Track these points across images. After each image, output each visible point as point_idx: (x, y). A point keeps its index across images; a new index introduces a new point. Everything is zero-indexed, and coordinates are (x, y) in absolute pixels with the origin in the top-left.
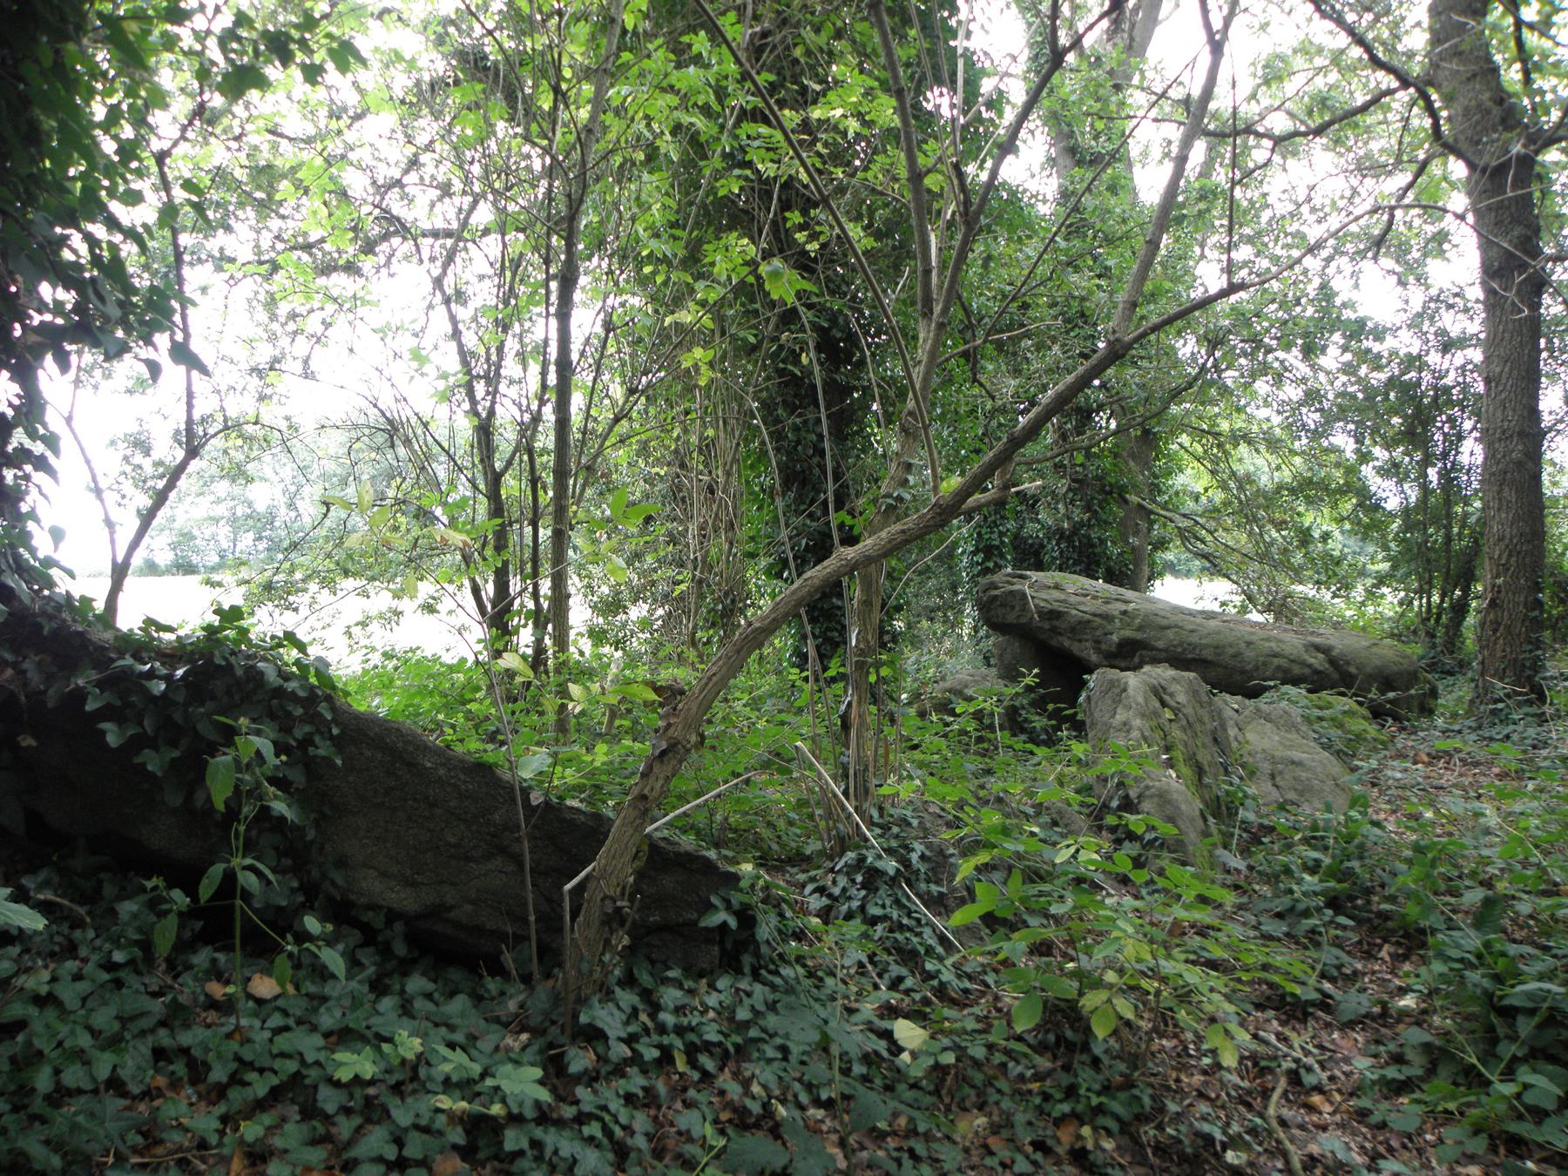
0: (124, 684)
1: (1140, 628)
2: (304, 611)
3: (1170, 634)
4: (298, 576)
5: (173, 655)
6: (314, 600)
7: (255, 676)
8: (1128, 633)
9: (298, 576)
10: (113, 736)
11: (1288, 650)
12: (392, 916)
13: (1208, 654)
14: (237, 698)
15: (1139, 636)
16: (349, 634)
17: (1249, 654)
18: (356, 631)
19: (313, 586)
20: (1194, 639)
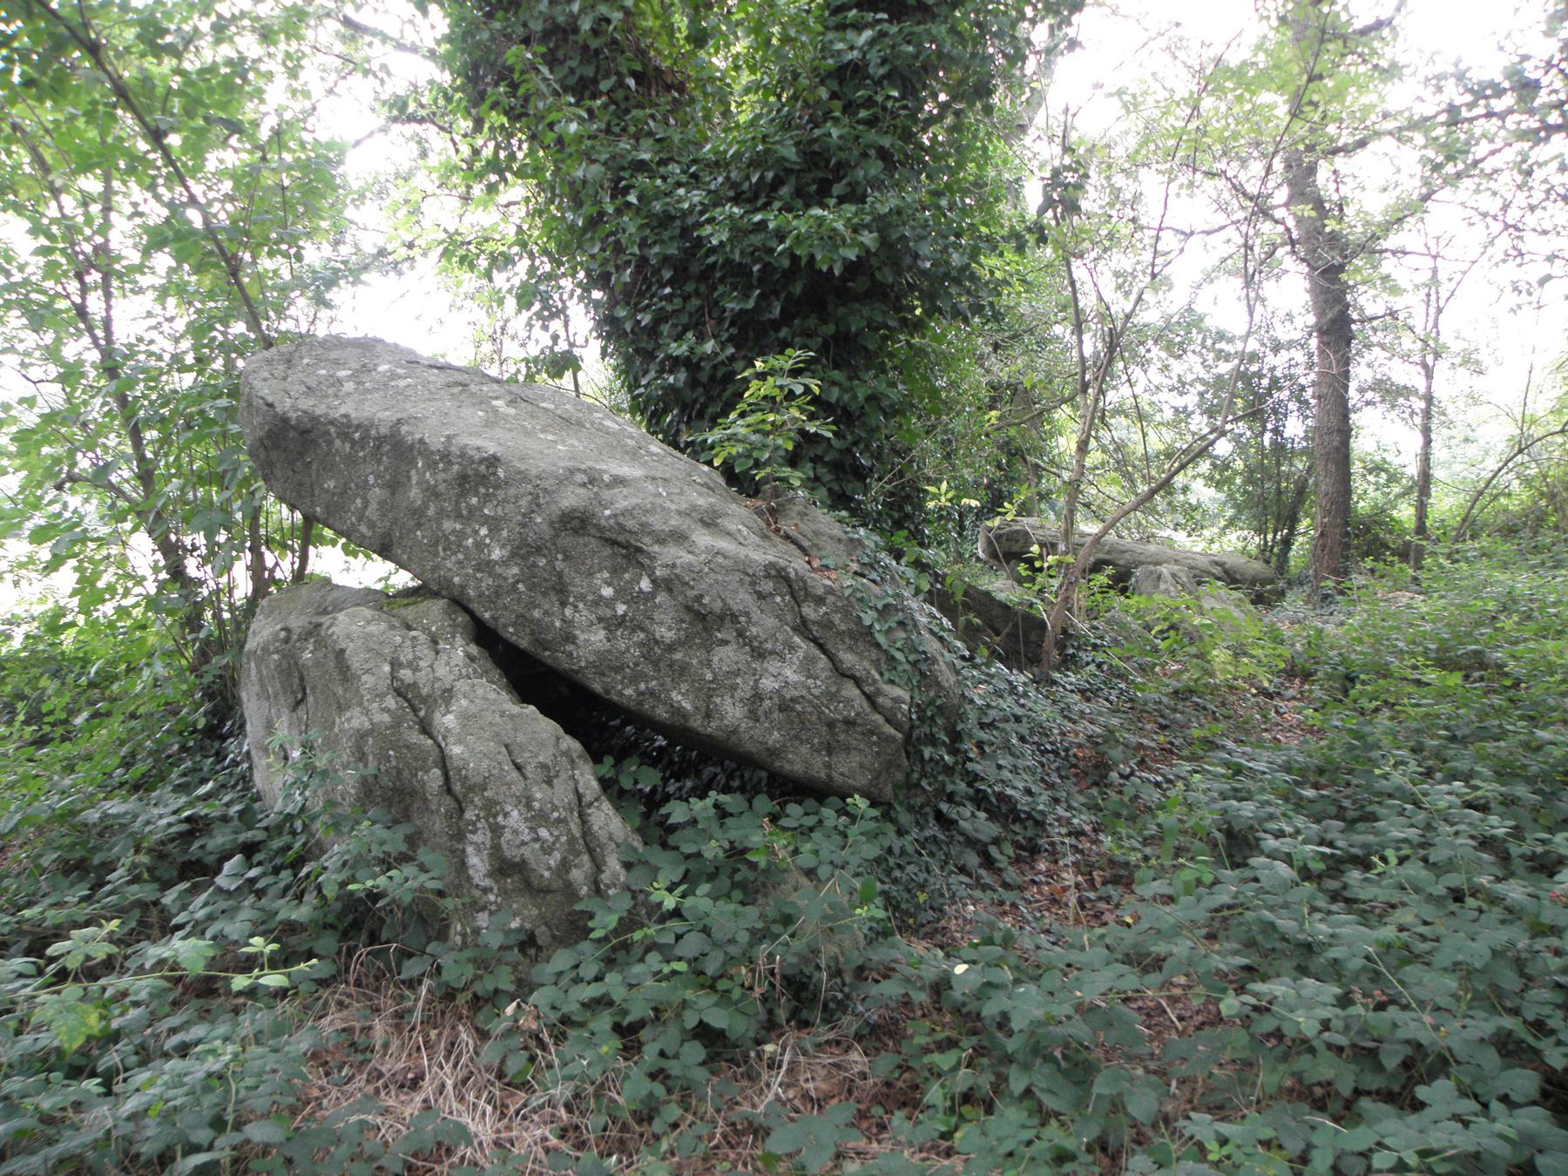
1: (1108, 552)
3: (1127, 555)
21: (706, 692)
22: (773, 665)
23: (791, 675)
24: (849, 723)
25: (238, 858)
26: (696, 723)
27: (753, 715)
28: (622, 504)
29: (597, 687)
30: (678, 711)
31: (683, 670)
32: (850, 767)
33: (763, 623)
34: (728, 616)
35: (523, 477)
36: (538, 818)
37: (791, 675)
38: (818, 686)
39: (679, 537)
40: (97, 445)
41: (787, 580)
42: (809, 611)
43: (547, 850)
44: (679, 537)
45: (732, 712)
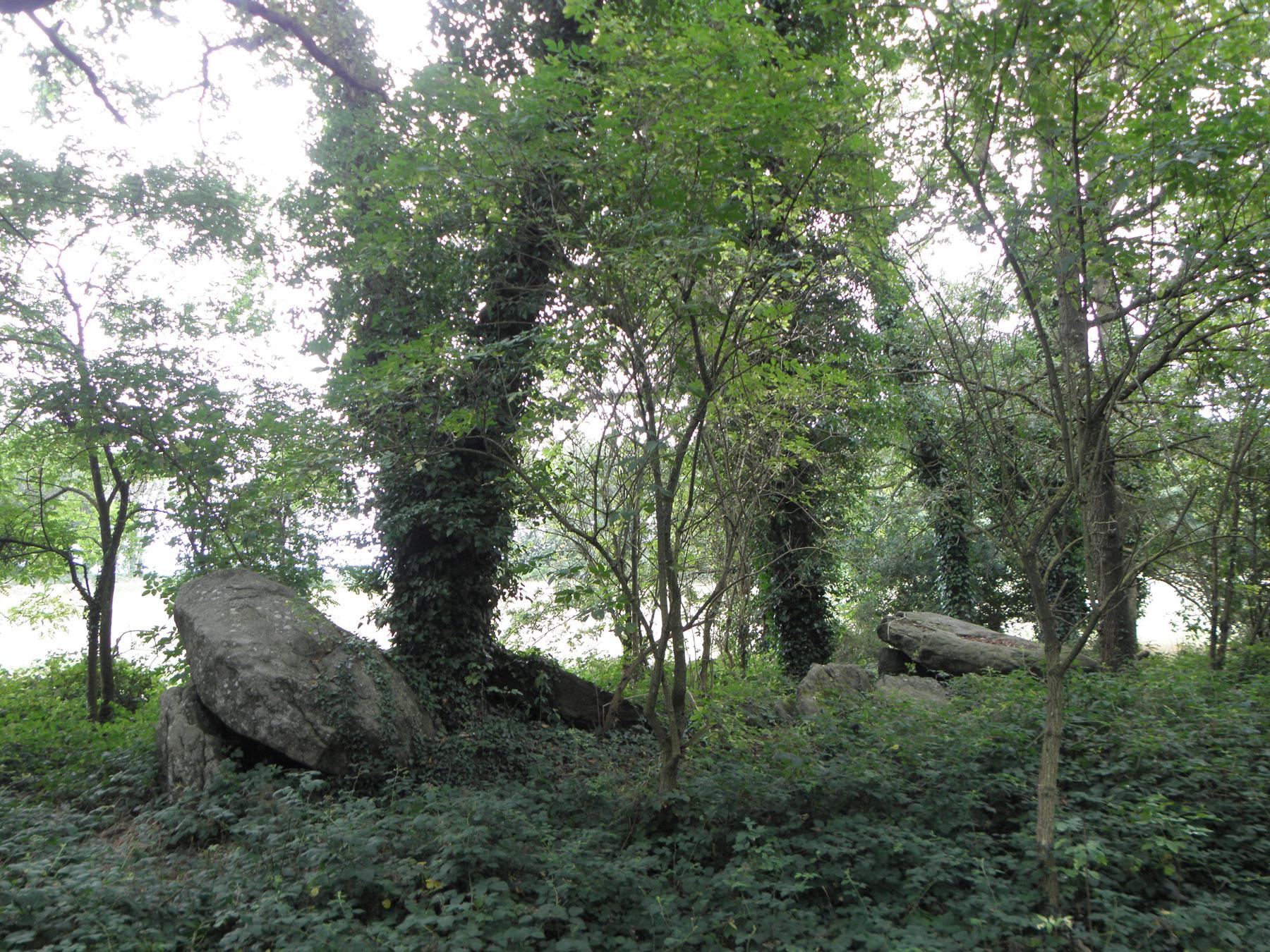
0: (516, 665)
1: (931, 645)
2: (545, 630)
3: (945, 647)
4: (541, 609)
5: (526, 658)
6: (550, 623)
7: (542, 663)
8: (925, 647)
9: (541, 609)
10: (514, 675)
11: (1002, 655)
12: (571, 718)
13: (962, 657)
14: (114, 871)
15: (930, 648)
16: (570, 642)
17: (982, 658)
18: (574, 640)
19: (549, 616)
20: (956, 650)
21: (255, 724)
22: (278, 716)
23: (285, 719)
24: (306, 740)
25: (521, 921)
26: (250, 735)
27: (270, 733)
28: (235, 654)
29: (229, 723)
30: (243, 730)
31: (244, 715)
32: (310, 757)
33: (274, 699)
34: (258, 697)
35: (209, 643)
36: (185, 763)
37: (285, 719)
38: (296, 725)
39: (249, 667)
40: (658, 384)
41: (287, 683)
42: (297, 696)
43: (187, 774)
44: (249, 667)
45: (263, 732)
